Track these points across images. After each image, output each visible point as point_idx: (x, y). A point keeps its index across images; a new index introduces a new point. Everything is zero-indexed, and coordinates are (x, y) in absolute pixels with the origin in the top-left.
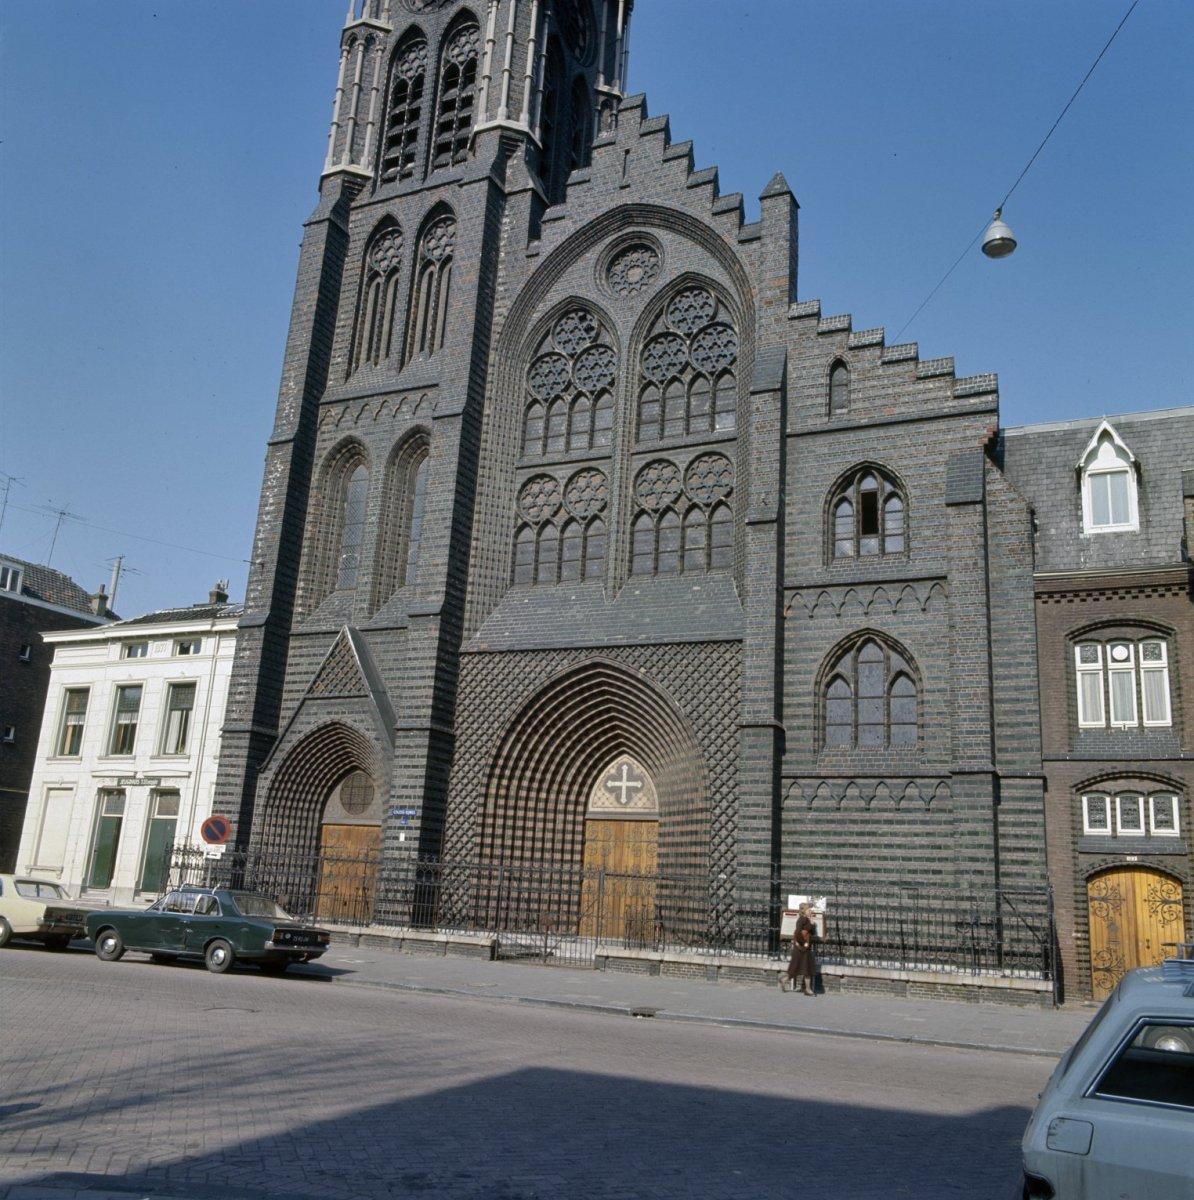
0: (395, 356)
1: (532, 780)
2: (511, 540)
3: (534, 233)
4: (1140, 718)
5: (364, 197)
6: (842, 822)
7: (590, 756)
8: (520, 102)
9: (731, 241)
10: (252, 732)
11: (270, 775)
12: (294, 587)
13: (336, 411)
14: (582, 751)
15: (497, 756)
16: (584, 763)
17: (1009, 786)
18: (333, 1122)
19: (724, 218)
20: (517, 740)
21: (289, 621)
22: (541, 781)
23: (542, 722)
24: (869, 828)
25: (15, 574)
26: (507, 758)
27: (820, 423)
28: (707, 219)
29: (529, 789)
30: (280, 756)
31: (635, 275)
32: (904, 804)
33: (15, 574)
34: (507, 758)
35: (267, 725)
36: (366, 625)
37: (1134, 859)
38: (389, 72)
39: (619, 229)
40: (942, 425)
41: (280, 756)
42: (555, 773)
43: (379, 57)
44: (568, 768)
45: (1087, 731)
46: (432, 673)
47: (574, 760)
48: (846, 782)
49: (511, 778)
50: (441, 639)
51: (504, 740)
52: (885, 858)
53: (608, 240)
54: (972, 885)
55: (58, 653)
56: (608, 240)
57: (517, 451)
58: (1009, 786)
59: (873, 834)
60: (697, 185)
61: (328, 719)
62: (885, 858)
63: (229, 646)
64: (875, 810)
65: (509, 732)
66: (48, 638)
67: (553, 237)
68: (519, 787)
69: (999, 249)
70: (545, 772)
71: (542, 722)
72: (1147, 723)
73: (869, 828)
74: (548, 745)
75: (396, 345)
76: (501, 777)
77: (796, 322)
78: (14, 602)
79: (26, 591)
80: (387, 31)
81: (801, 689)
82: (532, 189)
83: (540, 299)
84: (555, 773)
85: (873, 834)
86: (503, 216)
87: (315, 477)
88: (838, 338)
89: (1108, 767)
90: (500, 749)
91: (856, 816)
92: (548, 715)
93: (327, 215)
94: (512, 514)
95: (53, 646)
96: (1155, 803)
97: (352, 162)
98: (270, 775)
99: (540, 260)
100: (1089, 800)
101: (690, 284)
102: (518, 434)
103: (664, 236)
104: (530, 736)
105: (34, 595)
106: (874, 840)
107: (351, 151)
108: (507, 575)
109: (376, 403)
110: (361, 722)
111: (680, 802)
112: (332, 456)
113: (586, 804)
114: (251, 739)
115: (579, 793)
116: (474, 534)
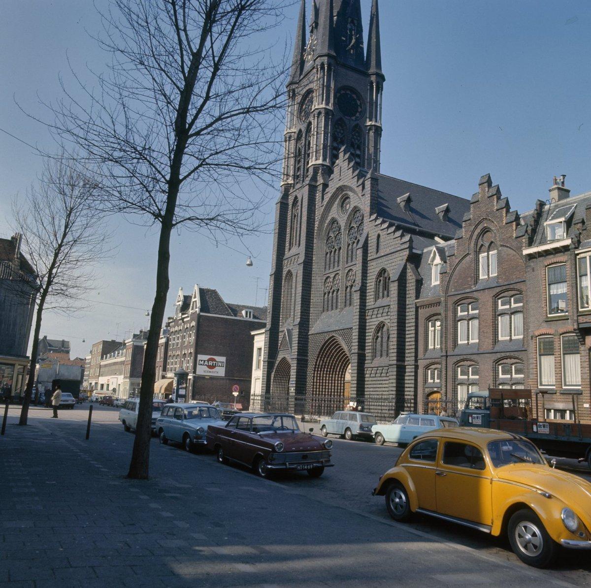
0: (297, 245)
1: (327, 371)
2: (322, 298)
3: (323, 199)
4: (511, 336)
5: (291, 191)
7: (343, 363)
10: (358, 353)
11: (273, 373)
12: (279, 317)
13: (286, 262)
14: (339, 362)
15: (316, 365)
16: (341, 365)
17: (408, 368)
18: (551, 537)
20: (321, 360)
21: (278, 328)
22: (330, 372)
23: (326, 354)
25: (250, 313)
26: (319, 365)
27: (375, 257)
29: (326, 374)
30: (275, 367)
31: (348, 206)
33: (250, 313)
34: (319, 365)
35: (303, 356)
37: (436, 389)
38: (296, 145)
39: (342, 193)
41: (275, 367)
42: (333, 369)
43: (293, 142)
44: (337, 367)
45: (503, 341)
47: (338, 364)
48: (371, 369)
49: (321, 371)
50: (299, 332)
51: (317, 360)
55: (256, 338)
57: (323, 270)
58: (408, 368)
63: (263, 337)
65: (318, 357)
66: (253, 333)
67: (327, 197)
68: (323, 374)
69: (251, 265)
70: (330, 369)
71: (326, 354)
72: (513, 338)
74: (330, 361)
76: (318, 371)
78: (251, 322)
79: (255, 317)
80: (295, 132)
83: (326, 219)
84: (333, 369)
86: (316, 193)
87: (283, 283)
89: (462, 357)
90: (316, 362)
91: (379, 379)
92: (328, 351)
93: (279, 201)
94: (322, 290)
95: (254, 335)
96: (515, 368)
97: (316, 160)
98: (273, 373)
100: (502, 368)
102: (324, 264)
104: (324, 358)
105: (258, 318)
107: (316, 156)
108: (322, 309)
109: (293, 258)
112: (286, 276)
113: (344, 378)
114: (358, 356)
115: (342, 375)
116: (311, 298)
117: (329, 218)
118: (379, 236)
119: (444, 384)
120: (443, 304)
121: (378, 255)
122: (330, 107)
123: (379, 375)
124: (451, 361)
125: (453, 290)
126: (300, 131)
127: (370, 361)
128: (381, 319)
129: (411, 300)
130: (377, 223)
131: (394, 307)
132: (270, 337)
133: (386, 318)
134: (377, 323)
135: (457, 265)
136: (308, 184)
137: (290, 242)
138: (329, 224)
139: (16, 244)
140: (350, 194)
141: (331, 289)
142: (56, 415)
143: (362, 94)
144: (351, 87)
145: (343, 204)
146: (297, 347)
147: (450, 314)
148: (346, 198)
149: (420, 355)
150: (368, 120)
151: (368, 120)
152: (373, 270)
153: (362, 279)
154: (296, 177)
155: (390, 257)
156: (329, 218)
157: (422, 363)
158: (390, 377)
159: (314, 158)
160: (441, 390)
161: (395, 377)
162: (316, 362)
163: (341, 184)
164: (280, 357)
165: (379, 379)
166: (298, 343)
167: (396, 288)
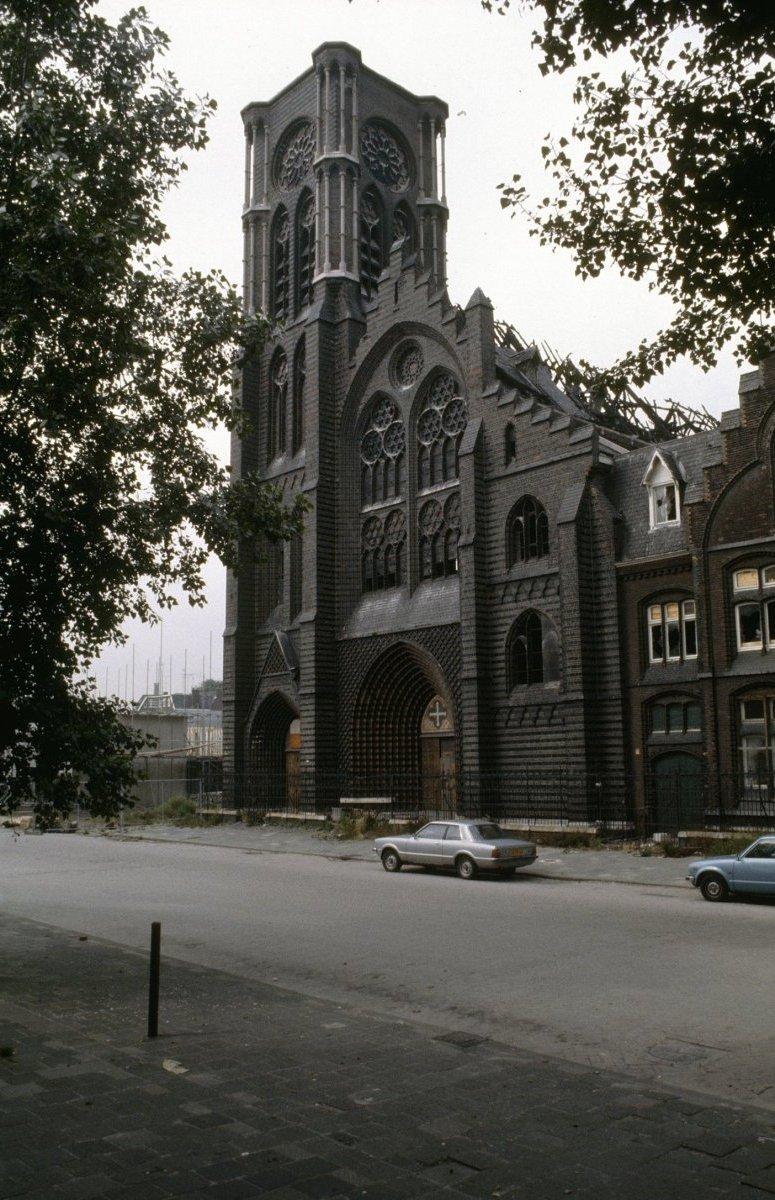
0: (289, 448)
6: (523, 734)
8: (339, 255)
9: (452, 342)
19: (448, 327)
24: (535, 737)
28: (439, 328)
31: (414, 367)
32: (553, 721)
36: (290, 628)
40: (562, 466)
45: (654, 665)
46: (313, 658)
48: (550, 707)
52: (544, 756)
53: (394, 347)
54: (575, 771)
56: (394, 347)
59: (537, 741)
60: (434, 304)
61: (273, 689)
62: (544, 756)
64: (524, 726)
67: (364, 349)
73: (535, 737)
75: (289, 438)
77: (487, 401)
80: (267, 211)
81: (307, 671)
82: (349, 319)
85: (537, 741)
88: (508, 409)
91: (529, 730)
94: (359, 545)
99: (357, 368)
101: (438, 375)
103: (422, 340)
106: (538, 745)
109: (290, 478)
110: (288, 690)
111: (565, 739)
117: (370, 393)
118: (510, 428)
119: (710, 735)
120: (697, 571)
121: (512, 469)
122: (354, 158)
123: (545, 721)
124: (725, 690)
125: (721, 539)
126: (281, 208)
127: (504, 694)
128: (528, 605)
129: (607, 562)
130: (503, 401)
131: (570, 577)
132: (238, 651)
133: (543, 601)
134: (517, 613)
135: (731, 485)
136: (319, 320)
137: (269, 444)
138: (368, 406)
139: (361, 206)
140: (422, 340)
141: (382, 543)
142: (685, 732)
143: (410, 140)
144: (388, 122)
145: (401, 362)
146: (313, 670)
147: (717, 590)
148: (411, 348)
149: (635, 679)
150: (422, 194)
151: (422, 194)
152: (504, 499)
153: (478, 514)
154: (273, 308)
155: (539, 473)
156: (370, 393)
157: (639, 695)
158: (571, 727)
159: (327, 264)
160: (705, 750)
161: (581, 726)
162: (358, 700)
163: (399, 319)
164: (265, 690)
165: (529, 730)
166: (316, 661)
167: (572, 538)
